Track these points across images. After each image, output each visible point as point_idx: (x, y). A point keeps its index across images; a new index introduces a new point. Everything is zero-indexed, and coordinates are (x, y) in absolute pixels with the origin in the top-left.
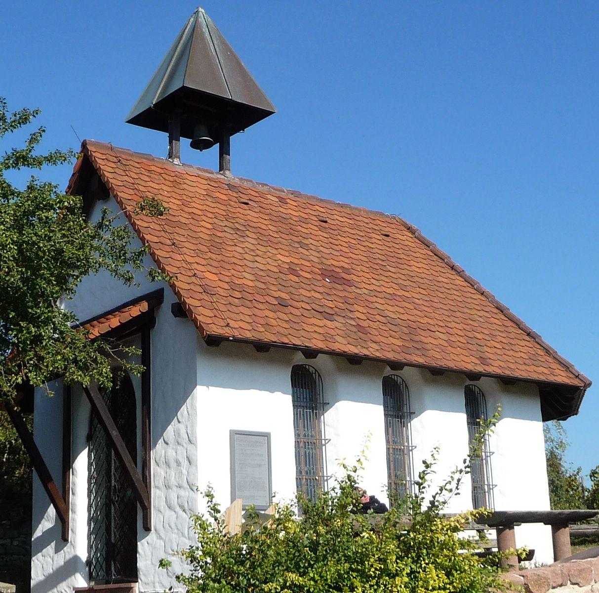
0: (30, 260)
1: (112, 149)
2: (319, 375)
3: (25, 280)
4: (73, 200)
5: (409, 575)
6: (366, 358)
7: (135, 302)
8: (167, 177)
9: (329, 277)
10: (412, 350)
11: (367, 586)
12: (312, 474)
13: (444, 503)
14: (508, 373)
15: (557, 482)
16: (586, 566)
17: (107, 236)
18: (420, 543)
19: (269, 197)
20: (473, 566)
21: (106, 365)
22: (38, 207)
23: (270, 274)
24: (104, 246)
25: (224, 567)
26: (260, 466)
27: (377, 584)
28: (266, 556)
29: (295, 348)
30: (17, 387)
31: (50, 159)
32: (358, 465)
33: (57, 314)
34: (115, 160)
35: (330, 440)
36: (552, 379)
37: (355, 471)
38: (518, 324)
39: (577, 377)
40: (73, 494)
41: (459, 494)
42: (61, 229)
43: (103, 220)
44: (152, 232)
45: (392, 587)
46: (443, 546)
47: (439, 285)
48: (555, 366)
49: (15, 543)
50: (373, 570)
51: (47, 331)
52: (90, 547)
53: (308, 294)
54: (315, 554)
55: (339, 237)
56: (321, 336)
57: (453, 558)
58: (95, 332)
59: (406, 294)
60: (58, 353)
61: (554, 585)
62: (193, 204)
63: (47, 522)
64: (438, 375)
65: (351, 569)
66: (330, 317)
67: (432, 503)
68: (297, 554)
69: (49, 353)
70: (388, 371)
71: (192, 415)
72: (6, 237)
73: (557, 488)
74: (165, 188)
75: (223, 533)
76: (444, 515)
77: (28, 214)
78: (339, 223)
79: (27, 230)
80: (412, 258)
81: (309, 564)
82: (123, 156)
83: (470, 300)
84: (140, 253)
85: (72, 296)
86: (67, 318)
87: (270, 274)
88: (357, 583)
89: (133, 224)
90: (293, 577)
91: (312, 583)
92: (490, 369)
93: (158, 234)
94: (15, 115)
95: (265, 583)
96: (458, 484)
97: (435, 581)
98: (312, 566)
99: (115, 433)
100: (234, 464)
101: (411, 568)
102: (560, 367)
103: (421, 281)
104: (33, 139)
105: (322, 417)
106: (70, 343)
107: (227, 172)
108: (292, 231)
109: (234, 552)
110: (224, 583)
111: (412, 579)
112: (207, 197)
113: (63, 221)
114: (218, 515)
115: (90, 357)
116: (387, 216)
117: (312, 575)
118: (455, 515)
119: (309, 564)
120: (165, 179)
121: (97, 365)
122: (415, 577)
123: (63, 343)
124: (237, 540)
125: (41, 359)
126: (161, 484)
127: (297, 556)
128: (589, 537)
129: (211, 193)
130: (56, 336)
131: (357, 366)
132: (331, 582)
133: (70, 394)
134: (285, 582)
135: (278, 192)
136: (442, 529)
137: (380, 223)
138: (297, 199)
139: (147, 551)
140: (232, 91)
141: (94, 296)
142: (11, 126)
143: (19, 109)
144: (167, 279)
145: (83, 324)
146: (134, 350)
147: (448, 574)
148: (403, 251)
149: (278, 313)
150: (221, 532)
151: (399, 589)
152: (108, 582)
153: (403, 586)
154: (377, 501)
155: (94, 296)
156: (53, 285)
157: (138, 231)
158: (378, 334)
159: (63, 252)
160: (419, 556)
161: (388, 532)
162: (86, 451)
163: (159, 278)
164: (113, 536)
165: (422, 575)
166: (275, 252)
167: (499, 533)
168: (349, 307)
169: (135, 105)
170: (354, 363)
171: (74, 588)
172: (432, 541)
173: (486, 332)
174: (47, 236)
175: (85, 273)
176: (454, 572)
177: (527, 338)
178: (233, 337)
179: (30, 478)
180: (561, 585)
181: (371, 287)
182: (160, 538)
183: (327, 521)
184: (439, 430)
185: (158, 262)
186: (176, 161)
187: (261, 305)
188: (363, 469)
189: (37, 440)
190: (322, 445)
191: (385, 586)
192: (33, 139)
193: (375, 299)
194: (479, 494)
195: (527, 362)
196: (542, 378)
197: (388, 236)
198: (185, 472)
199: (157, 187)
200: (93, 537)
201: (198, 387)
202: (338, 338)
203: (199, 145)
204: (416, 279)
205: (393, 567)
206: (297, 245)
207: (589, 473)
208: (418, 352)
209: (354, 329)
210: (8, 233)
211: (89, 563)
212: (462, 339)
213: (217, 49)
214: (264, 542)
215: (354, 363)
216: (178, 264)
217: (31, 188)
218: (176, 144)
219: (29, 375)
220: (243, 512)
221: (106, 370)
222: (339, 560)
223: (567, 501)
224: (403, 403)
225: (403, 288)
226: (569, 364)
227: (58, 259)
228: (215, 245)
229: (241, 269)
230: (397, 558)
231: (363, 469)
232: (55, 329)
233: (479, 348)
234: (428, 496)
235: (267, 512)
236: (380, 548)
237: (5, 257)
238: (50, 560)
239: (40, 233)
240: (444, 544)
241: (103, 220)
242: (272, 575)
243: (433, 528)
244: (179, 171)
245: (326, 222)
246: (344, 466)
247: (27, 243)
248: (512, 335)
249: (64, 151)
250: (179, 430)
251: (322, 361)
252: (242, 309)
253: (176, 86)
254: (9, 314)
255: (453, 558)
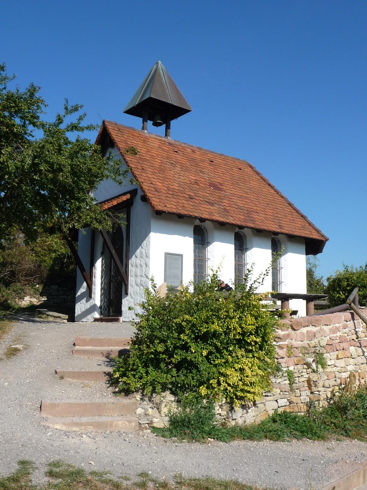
0: (76, 173)
1: (116, 124)
2: (206, 230)
3: (74, 182)
4: (96, 147)
5: (238, 318)
6: (227, 223)
7: (124, 194)
8: (141, 138)
9: (213, 187)
10: (249, 221)
11: (220, 322)
12: (201, 273)
13: (256, 288)
14: (291, 233)
15: (311, 282)
16: (319, 318)
17: (112, 163)
18: (244, 305)
19: (187, 149)
20: (267, 316)
21: (109, 221)
22: (80, 149)
23: (186, 184)
24: (110, 168)
25: (157, 311)
26: (178, 268)
27: (224, 321)
28: (176, 307)
29: (196, 218)
30: (69, 229)
31: (87, 128)
32: (218, 269)
33: (88, 197)
34: (117, 129)
35: (210, 259)
36: (311, 236)
37: (217, 272)
38: (297, 211)
39: (322, 236)
40: (95, 277)
41: (263, 284)
42: (91, 160)
43: (110, 156)
44: (133, 163)
45: (231, 323)
46: (255, 306)
47: (263, 192)
48: (313, 231)
49: (69, 298)
50: (222, 315)
51: (83, 205)
52: (101, 301)
53: (203, 194)
54: (197, 307)
55: (218, 169)
56: (208, 213)
57: (258, 312)
58: (106, 207)
59: (248, 196)
60: (88, 215)
61: (304, 326)
62: (153, 151)
63: (83, 289)
64: (260, 233)
65: (213, 314)
66: (212, 204)
67: (250, 287)
68: (190, 307)
69: (84, 215)
70: (237, 230)
71: (148, 245)
72: (65, 162)
73: (311, 284)
74: (140, 143)
75: (158, 297)
76: (256, 293)
77: (77, 153)
78: (219, 163)
79: (75, 159)
80: (251, 180)
81: (195, 311)
82: (121, 128)
83: (276, 200)
84: (126, 171)
85: (96, 190)
86: (93, 200)
87: (186, 184)
88: (215, 321)
89: (125, 159)
90: (187, 317)
91: (195, 320)
92: (283, 231)
93: (136, 164)
94: (72, 107)
95: (175, 319)
96: (263, 280)
97: (250, 321)
98: (196, 313)
99: (113, 252)
100: (166, 267)
101: (240, 316)
102: (314, 231)
103: (255, 190)
104: (81, 119)
105: (207, 249)
106: (93, 211)
107: (169, 137)
108: (197, 165)
109: (162, 305)
110: (157, 318)
111: (240, 320)
112: (159, 148)
113: (91, 157)
114: (156, 289)
115: (102, 217)
116: (241, 160)
117: (195, 316)
118: (260, 294)
119: (195, 311)
120: (140, 139)
121: (105, 221)
122: (241, 319)
123: (91, 211)
124: (164, 300)
125: (80, 217)
126: (133, 275)
127: (191, 307)
128: (324, 306)
129: (161, 147)
130: (88, 208)
131: (223, 227)
132: (204, 320)
133: (94, 233)
134: (184, 319)
135: (191, 147)
136: (255, 299)
137: (238, 163)
138: (200, 151)
139: (126, 303)
140: (172, 100)
141: (105, 191)
142: (70, 112)
143: (74, 104)
144: (139, 183)
145: (100, 203)
146: (123, 215)
147: (256, 319)
148: (248, 177)
149: (189, 202)
150: (156, 296)
151: (234, 324)
152: (109, 316)
153: (236, 323)
154: (229, 286)
155: (105, 191)
156: (87, 184)
157: (127, 162)
158: (233, 213)
159: (92, 170)
160: (243, 311)
161: (230, 299)
162: (101, 259)
163: (135, 183)
164: (111, 296)
165: (244, 318)
166: (188, 174)
167: (282, 303)
168: (221, 200)
169: (128, 104)
170: (222, 226)
171: (94, 318)
172: (250, 304)
173: (283, 214)
174: (87, 161)
175: (102, 180)
176: (259, 318)
177: (301, 218)
178: (168, 211)
179: (76, 270)
180: (307, 326)
181: (232, 192)
182: (132, 298)
183: (204, 294)
184: (259, 256)
185: (135, 177)
186: (146, 131)
187: (181, 198)
188: (220, 271)
189: (79, 253)
190: (206, 261)
191: (228, 322)
192: (81, 119)
193: (233, 197)
194: (275, 284)
195: (301, 228)
196: (307, 236)
197: (241, 169)
198: (144, 270)
199: (136, 142)
200: (103, 296)
201: (151, 233)
202: (215, 214)
203: (156, 124)
204: (252, 189)
205: (231, 315)
206: (199, 172)
207: (326, 278)
208: (251, 222)
209: (223, 211)
210: (66, 160)
211: (101, 307)
212: (271, 217)
213: (166, 81)
214: (175, 301)
215: (222, 226)
216: (144, 178)
217: (77, 141)
218: (146, 124)
219: (75, 224)
220: (167, 288)
221: (109, 223)
222: (208, 310)
223: (316, 291)
224: (243, 244)
225: (246, 193)
226: (320, 230)
227: (89, 173)
228: (162, 170)
229: (173, 181)
230: (234, 311)
231: (220, 271)
232: (87, 205)
233: (279, 221)
234: (249, 285)
235: (177, 289)
236: (226, 306)
237: (65, 171)
238: (84, 305)
239: (81, 161)
240: (255, 306)
241: (110, 156)
242: (178, 316)
243: (251, 299)
244: (147, 136)
245: (213, 162)
246: (212, 270)
247: (75, 165)
248: (295, 216)
249: (94, 125)
250: (142, 251)
251: (207, 224)
252: (172, 199)
253: (146, 97)
254: (66, 196)
255: (258, 312)
